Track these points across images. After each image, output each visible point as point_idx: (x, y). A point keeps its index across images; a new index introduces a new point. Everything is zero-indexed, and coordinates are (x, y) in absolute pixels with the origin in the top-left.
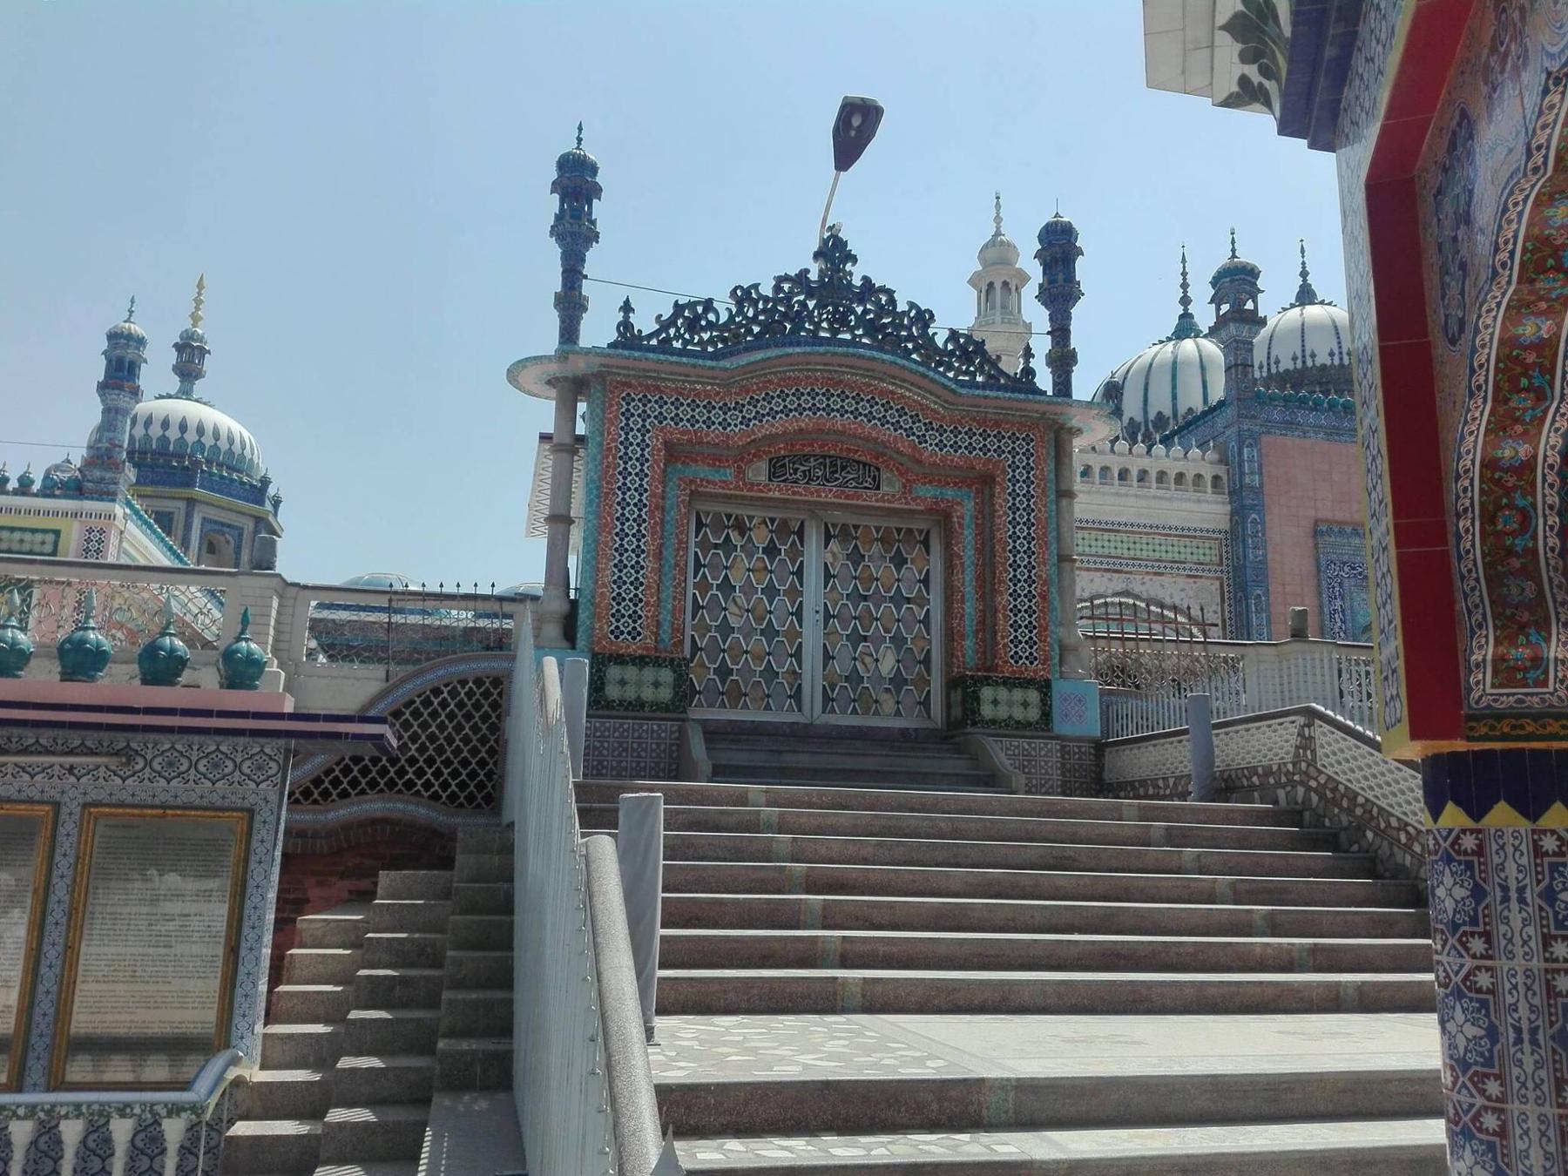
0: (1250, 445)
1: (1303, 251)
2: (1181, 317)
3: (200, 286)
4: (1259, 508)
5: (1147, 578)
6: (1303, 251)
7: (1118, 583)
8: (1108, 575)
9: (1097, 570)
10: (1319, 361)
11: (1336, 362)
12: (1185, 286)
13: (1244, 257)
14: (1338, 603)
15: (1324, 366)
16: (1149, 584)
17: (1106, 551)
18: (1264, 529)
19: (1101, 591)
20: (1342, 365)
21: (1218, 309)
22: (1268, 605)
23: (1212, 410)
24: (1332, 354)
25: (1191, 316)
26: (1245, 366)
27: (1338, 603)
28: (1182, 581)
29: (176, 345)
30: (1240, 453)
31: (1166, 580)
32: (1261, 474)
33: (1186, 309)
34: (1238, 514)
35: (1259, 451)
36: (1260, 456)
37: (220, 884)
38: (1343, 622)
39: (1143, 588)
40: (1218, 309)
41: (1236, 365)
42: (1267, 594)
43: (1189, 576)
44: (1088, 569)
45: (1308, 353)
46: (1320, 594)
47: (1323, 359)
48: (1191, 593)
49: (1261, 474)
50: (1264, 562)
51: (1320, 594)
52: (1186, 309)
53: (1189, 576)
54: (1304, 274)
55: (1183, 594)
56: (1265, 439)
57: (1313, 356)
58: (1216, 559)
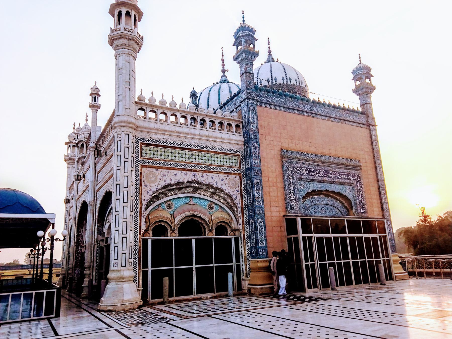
1: (269, 43)
2: (222, 77)
4: (257, 140)
5: (205, 174)
6: (269, 43)
7: (190, 176)
8: (184, 172)
9: (179, 169)
11: (285, 82)
13: (365, 62)
14: (292, 185)
15: (280, 84)
16: (206, 177)
18: (259, 150)
19: (181, 180)
20: (287, 84)
21: (237, 48)
22: (262, 187)
23: (235, 96)
24: (283, 79)
27: (292, 185)
28: (222, 176)
30: (249, 114)
31: (214, 175)
34: (247, 142)
36: (257, 115)
37: (54, 261)
43: (225, 173)
44: (174, 169)
46: (284, 182)
47: (279, 81)
48: (226, 182)
50: (260, 165)
51: (284, 182)
54: (270, 52)
55: (222, 182)
56: (259, 108)
57: (276, 79)
58: (238, 165)
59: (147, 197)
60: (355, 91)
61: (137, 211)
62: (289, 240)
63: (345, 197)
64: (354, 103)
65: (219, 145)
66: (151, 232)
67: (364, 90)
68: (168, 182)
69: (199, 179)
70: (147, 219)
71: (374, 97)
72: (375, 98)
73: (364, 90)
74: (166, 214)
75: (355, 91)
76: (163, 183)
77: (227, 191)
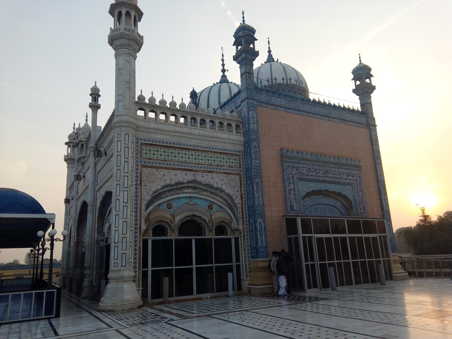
0: (252, 110)
1: (269, 42)
2: (222, 77)
3: (243, 13)
5: (205, 174)
6: (269, 42)
7: (189, 177)
8: (184, 172)
10: (278, 82)
11: (285, 82)
12: (223, 65)
14: (292, 185)
17: (170, 151)
18: (259, 150)
19: (181, 180)
22: (262, 187)
23: (235, 95)
24: (283, 79)
25: (226, 76)
26: (250, 73)
27: (292, 185)
28: (222, 176)
29: (66, 144)
30: (249, 114)
31: (214, 175)
32: (257, 124)
33: (224, 74)
35: (257, 113)
38: (295, 195)
39: (202, 179)
40: (237, 48)
41: (246, 72)
42: (261, 181)
43: (225, 173)
45: (273, 78)
46: (284, 182)
47: (280, 81)
48: (226, 182)
49: (257, 124)
52: (224, 74)
53: (225, 173)
54: (270, 52)
55: (222, 182)
56: (259, 108)
58: (238, 165)
59: (147, 197)
60: (354, 91)
61: (137, 210)
62: (289, 240)
63: (345, 197)
64: (354, 102)
65: (219, 145)
66: (151, 232)
67: (364, 89)
68: (168, 182)
69: (200, 178)
70: (148, 219)
71: (374, 97)
72: (375, 98)
73: (364, 89)
74: (166, 214)
75: (354, 91)
76: (163, 183)
77: (227, 191)
